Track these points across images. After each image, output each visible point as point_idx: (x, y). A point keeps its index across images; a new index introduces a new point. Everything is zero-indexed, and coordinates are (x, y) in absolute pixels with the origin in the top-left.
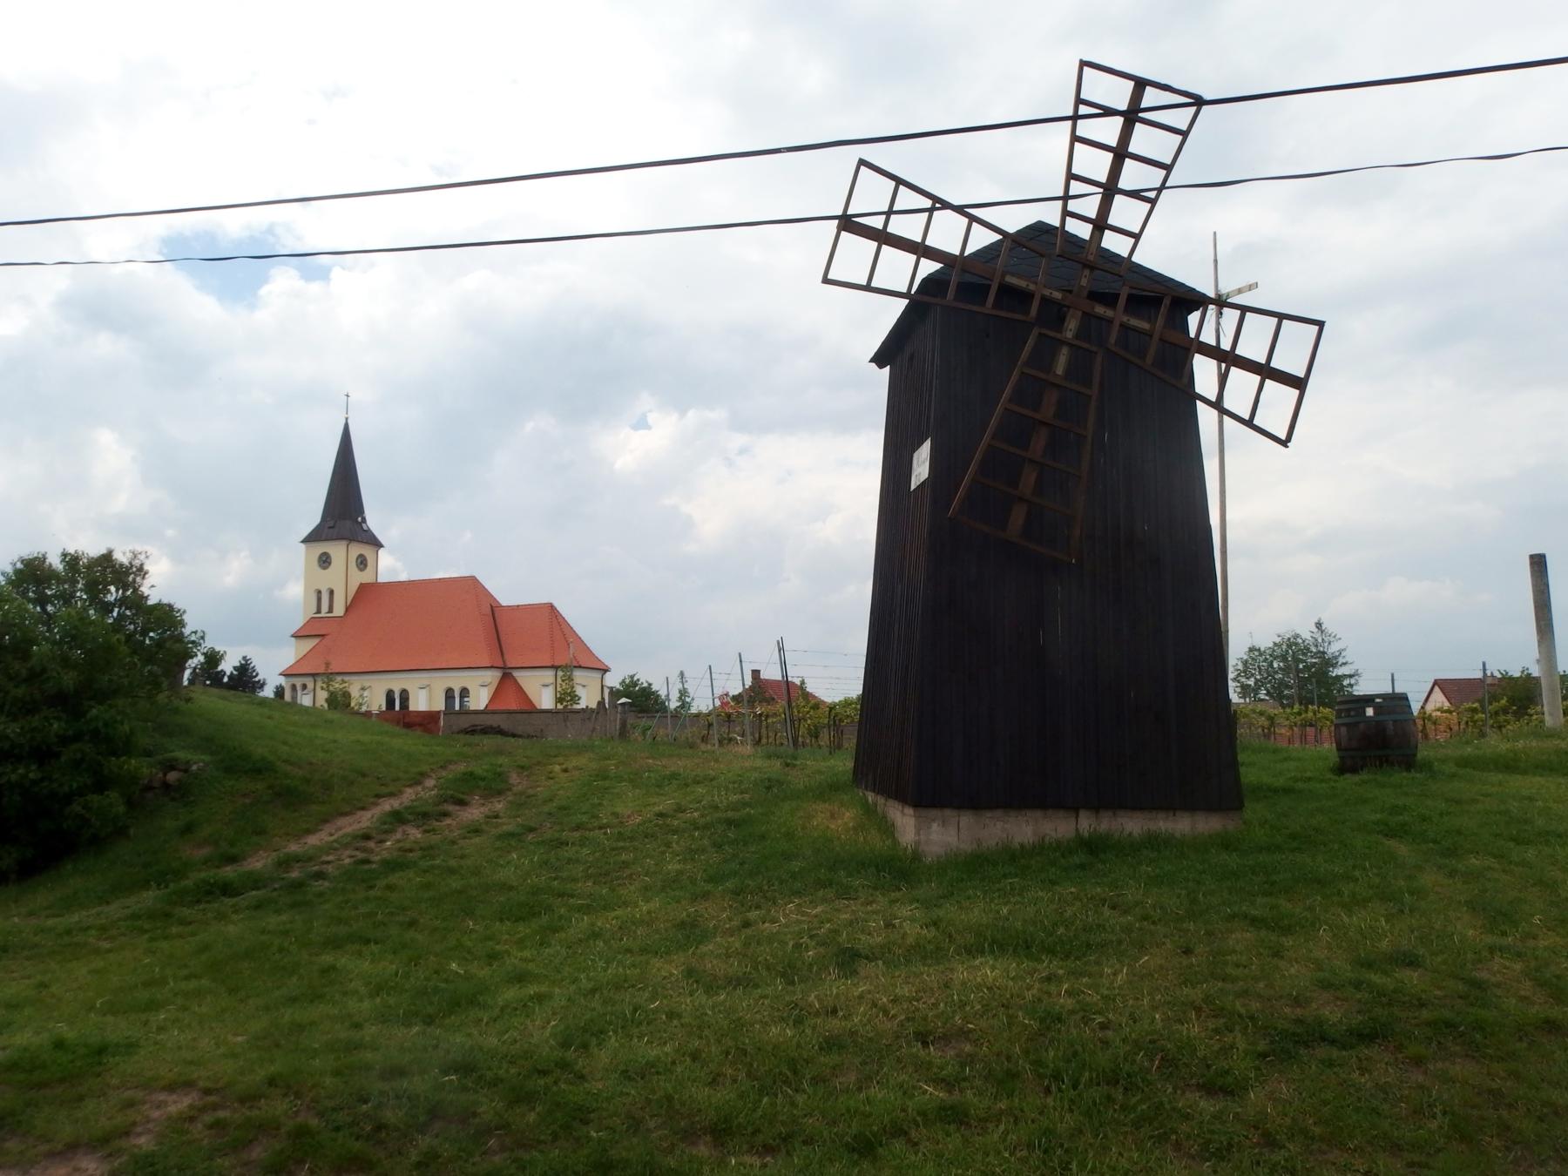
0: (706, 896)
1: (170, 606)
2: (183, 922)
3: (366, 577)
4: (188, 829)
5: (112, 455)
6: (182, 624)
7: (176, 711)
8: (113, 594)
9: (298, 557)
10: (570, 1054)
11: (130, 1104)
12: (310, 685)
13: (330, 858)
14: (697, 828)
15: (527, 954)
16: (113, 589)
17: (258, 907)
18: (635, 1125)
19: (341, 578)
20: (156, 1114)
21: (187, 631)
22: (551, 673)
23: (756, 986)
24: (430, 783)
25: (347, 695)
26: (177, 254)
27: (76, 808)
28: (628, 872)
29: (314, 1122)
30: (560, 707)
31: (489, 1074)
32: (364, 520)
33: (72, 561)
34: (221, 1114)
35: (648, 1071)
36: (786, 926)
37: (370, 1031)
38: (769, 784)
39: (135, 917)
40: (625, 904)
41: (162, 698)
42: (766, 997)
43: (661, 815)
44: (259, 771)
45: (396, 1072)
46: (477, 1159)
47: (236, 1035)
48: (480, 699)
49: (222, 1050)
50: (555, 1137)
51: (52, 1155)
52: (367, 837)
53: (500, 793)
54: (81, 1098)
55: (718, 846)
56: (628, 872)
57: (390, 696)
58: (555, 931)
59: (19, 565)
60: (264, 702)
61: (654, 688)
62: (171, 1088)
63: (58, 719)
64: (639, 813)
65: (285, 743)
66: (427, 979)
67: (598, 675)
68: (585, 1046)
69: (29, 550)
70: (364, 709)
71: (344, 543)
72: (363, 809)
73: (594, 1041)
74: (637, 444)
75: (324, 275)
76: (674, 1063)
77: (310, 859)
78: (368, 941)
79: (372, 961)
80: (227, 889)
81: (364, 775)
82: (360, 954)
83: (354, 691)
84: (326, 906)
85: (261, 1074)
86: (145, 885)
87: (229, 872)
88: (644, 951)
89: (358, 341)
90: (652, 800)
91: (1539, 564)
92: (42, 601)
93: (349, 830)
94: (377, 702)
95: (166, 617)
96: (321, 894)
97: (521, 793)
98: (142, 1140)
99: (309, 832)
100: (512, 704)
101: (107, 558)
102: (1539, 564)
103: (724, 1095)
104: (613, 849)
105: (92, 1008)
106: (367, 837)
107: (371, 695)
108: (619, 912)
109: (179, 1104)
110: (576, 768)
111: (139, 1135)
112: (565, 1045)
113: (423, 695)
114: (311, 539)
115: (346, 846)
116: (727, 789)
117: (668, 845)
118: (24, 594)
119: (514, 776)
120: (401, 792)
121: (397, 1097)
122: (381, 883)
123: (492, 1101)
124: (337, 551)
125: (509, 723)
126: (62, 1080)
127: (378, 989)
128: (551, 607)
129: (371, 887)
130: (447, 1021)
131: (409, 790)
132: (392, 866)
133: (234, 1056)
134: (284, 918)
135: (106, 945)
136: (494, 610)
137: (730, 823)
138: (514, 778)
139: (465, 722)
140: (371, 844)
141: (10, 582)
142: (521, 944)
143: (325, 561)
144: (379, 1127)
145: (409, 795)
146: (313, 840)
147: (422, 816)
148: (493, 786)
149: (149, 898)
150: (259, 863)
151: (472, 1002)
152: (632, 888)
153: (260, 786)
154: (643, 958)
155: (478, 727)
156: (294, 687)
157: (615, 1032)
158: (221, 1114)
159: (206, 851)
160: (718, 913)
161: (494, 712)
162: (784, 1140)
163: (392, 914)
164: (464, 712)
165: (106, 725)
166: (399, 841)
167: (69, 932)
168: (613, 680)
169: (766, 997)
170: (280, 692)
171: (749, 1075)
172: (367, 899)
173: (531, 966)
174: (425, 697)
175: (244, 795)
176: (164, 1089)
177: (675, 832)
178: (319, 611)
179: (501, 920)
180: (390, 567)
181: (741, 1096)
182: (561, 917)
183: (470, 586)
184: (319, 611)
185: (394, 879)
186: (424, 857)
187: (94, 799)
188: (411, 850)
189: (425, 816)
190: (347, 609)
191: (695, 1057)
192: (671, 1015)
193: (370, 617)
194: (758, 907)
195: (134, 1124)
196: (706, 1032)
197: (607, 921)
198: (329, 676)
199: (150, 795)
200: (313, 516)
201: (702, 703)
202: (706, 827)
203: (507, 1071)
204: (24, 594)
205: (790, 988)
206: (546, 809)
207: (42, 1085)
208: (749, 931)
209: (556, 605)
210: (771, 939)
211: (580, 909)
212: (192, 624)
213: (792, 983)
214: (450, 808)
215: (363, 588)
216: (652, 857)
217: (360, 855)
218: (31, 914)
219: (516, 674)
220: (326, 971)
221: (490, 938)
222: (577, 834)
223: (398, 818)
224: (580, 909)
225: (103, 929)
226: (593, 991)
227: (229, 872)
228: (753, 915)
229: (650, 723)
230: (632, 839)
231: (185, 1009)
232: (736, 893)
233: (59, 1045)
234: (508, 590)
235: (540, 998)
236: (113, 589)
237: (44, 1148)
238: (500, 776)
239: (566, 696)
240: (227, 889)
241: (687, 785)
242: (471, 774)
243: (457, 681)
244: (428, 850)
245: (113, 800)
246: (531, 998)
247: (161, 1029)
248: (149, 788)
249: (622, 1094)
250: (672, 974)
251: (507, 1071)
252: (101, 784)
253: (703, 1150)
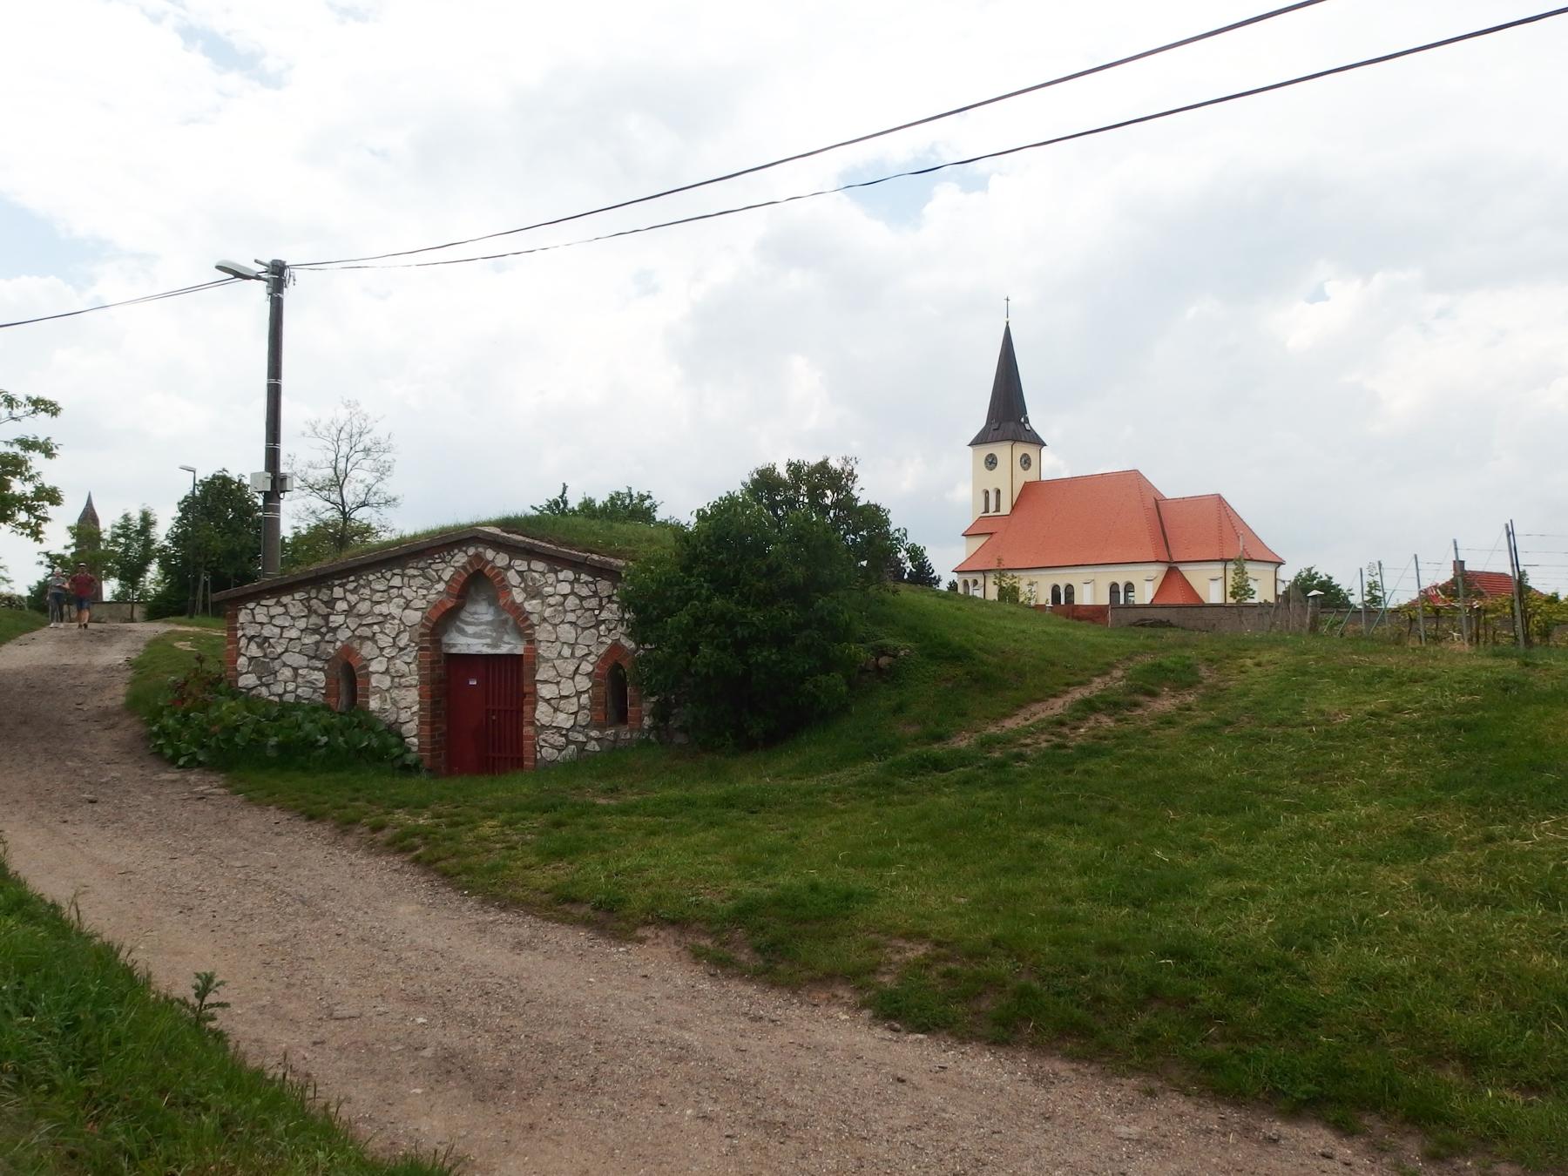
0: (1436, 804)
1: (877, 508)
2: (902, 791)
3: (1031, 476)
4: (899, 709)
5: (804, 378)
6: (887, 522)
7: (883, 602)
8: (829, 497)
9: (967, 460)
10: (1292, 955)
11: (874, 947)
12: (981, 582)
13: (1029, 741)
14: (1418, 731)
15: (1233, 848)
16: (829, 493)
17: (966, 783)
18: (1371, 1037)
19: (1007, 478)
20: (897, 958)
21: (892, 529)
22: (1219, 567)
23: (1508, 907)
24: (1118, 673)
25: (1015, 590)
26: (864, 184)
27: (808, 686)
28: (1339, 773)
29: (1036, 985)
30: (1231, 600)
31: (1207, 963)
32: (1027, 421)
33: (795, 469)
34: (952, 966)
35: (1382, 982)
36: (1541, 844)
37: (1082, 907)
38: (1506, 686)
39: (862, 784)
40: (1339, 806)
41: (872, 590)
42: (1522, 920)
43: (1373, 714)
44: (958, 658)
45: (1113, 949)
46: (1197, 1044)
47: (958, 896)
48: (1145, 594)
49: (947, 909)
50: (1281, 1036)
51: (812, 980)
52: (1062, 724)
53: (1190, 686)
54: (834, 936)
55: (1447, 752)
56: (1339, 773)
57: (1055, 591)
58: (1262, 828)
60: (939, 594)
61: (1335, 582)
62: (907, 936)
63: (792, 608)
64: (1349, 711)
65: (979, 633)
66: (1133, 863)
67: (1271, 568)
68: (1308, 948)
69: (761, 464)
70: (1033, 603)
72: (1055, 696)
73: (1317, 945)
74: (1311, 320)
75: (981, 184)
76: (1412, 978)
77: (1009, 741)
78: (1071, 822)
79: (1077, 842)
80: (938, 765)
81: (1053, 664)
82: (1065, 834)
83: (1023, 587)
84: (1028, 787)
85: (986, 934)
86: (869, 756)
87: (937, 749)
88: (1366, 856)
89: (1014, 248)
90: (1363, 698)
92: (773, 506)
93: (1042, 716)
94: (1045, 597)
95: (874, 517)
96: (1022, 775)
97: (1214, 686)
98: (886, 979)
99: (1006, 716)
100: (1178, 598)
101: (823, 466)
103: (1475, 1021)
104: (1321, 748)
105: (835, 860)
106: (1062, 724)
107: (1038, 588)
108: (1332, 814)
109: (916, 952)
110: (1270, 662)
111: (884, 974)
112: (1286, 944)
113: (1088, 589)
114: (978, 441)
115: (1042, 731)
116: (1452, 689)
117: (1385, 747)
118: (759, 501)
119: (1203, 669)
120: (1091, 682)
121: (1115, 972)
122: (1080, 767)
123: (1211, 989)
124: (1002, 451)
125: (1178, 614)
126: (818, 919)
127: (1084, 870)
128: (1219, 498)
129: (1070, 771)
130: (1156, 906)
131: (1097, 680)
132: (1088, 752)
133: (958, 914)
134: (991, 793)
135: (841, 807)
136: (1159, 503)
137: (1458, 726)
138: (1203, 671)
139: (1133, 616)
140: (1066, 730)
141: (749, 491)
142: (1226, 836)
143: (991, 462)
144: (1099, 999)
145: (1098, 684)
146: (1010, 724)
147: (1110, 705)
148: (1183, 678)
149: (871, 768)
150: (962, 742)
151: (1181, 890)
152: (1346, 790)
153: (960, 672)
154: (1366, 864)
155: (1149, 621)
156: (966, 583)
157: (1340, 938)
158: (952, 966)
159: (913, 730)
160: (1452, 822)
161: (1163, 607)
162: (1554, 1080)
163: (1091, 798)
164: (1130, 607)
165: (830, 614)
166: (1091, 728)
167: (810, 793)
168: (1288, 574)
169: (1522, 920)
170: (953, 586)
171: (1506, 1002)
172: (1067, 782)
173: (1239, 861)
174: (1091, 591)
175: (947, 680)
176: (901, 936)
177: (1392, 733)
178: (987, 511)
179: (1203, 812)
180: (1053, 465)
181: (1497, 1024)
182: (1267, 814)
183: (1133, 479)
184: (987, 511)
185: (1091, 764)
186: (1117, 745)
187: (822, 678)
188: (1106, 738)
189: (1116, 704)
191: (1438, 975)
192: (1405, 928)
193: (1034, 515)
194: (1503, 821)
195: (879, 963)
196: (1451, 950)
197: (1323, 822)
198: (1001, 572)
199: (865, 677)
201: (1400, 592)
202: (1429, 730)
203: (1225, 963)
204: (759, 501)
205: (1554, 914)
206: (1241, 704)
207: (803, 921)
208: (1494, 847)
209: (1224, 496)
210: (1523, 857)
211: (1288, 807)
212: (896, 523)
213: (1557, 909)
214: (1141, 698)
215: (1027, 487)
216: (1366, 759)
217: (1056, 740)
218: (778, 775)
219: (1182, 568)
220: (1035, 846)
221: (1191, 829)
222: (1279, 731)
223: (1090, 706)
224: (1288, 807)
225: (837, 792)
226: (1312, 893)
227: (937, 749)
228: (1498, 829)
229: (1339, 618)
230: (1342, 738)
231: (912, 868)
232: (1474, 803)
233: (814, 888)
234: (1172, 483)
235: (1253, 894)
236: (829, 493)
237: (806, 974)
238: (1190, 668)
239: (1241, 590)
240: (938, 765)
241: (1402, 683)
242: (1160, 665)
243: (1121, 576)
244: (1122, 739)
245: (836, 680)
246: (1243, 893)
247: (893, 884)
248: (864, 671)
249: (1352, 1002)
250: (1401, 884)
251: (1225, 963)
252: (828, 666)
253: (1451, 1075)
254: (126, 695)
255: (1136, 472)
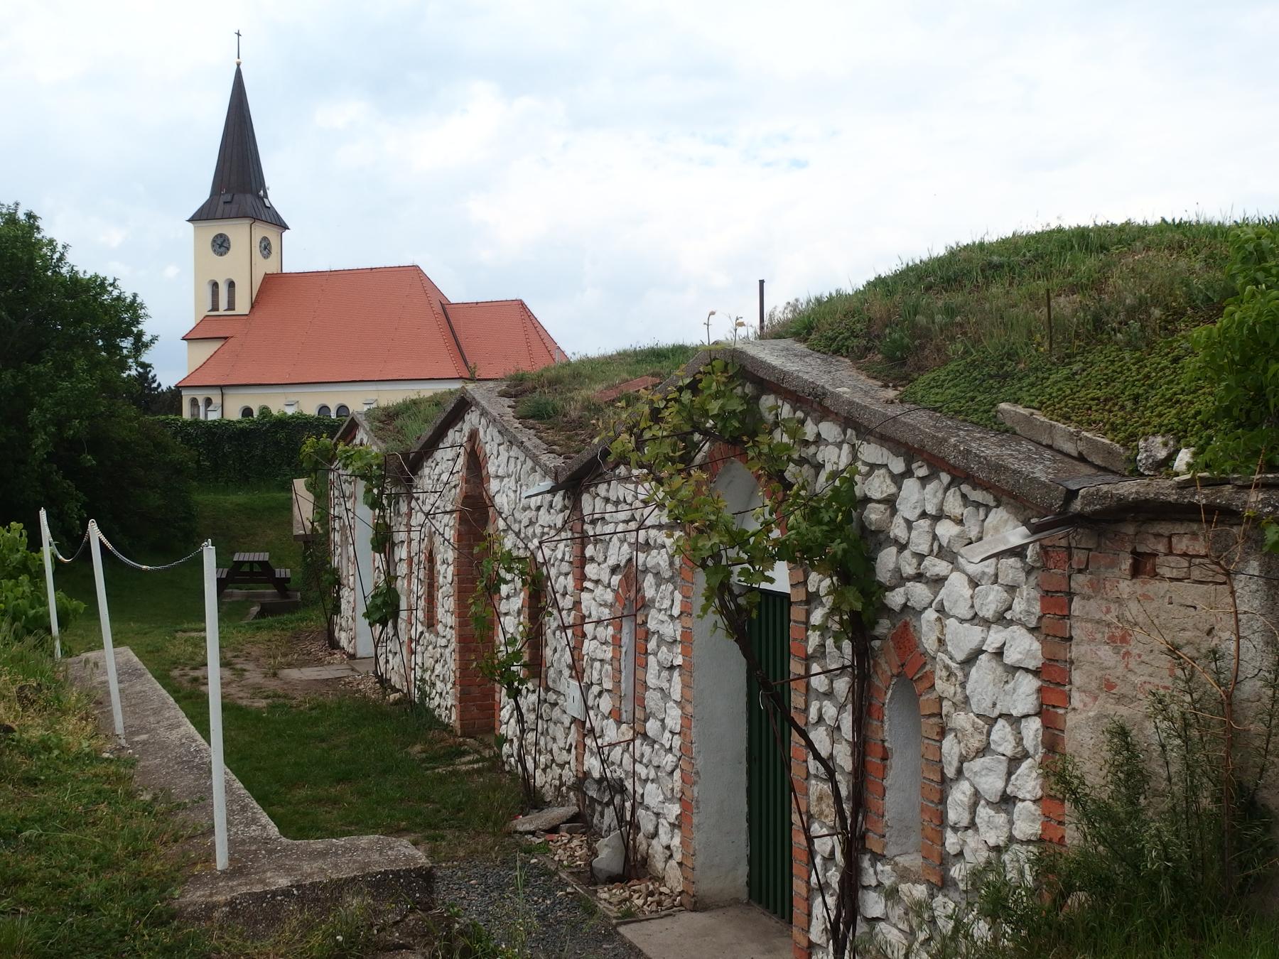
3: (270, 266)
12: (216, 400)
19: (241, 267)
59: (834, 294)
71: (247, 222)
78: (1081, 458)
91: (762, 282)
102: (762, 282)
114: (200, 217)
124: (238, 232)
128: (522, 304)
143: (221, 245)
178: (215, 307)
180: (302, 252)
184: (215, 307)
190: (252, 307)
200: (201, 192)
215: (269, 279)
254: (492, 499)
255: (416, 269)
